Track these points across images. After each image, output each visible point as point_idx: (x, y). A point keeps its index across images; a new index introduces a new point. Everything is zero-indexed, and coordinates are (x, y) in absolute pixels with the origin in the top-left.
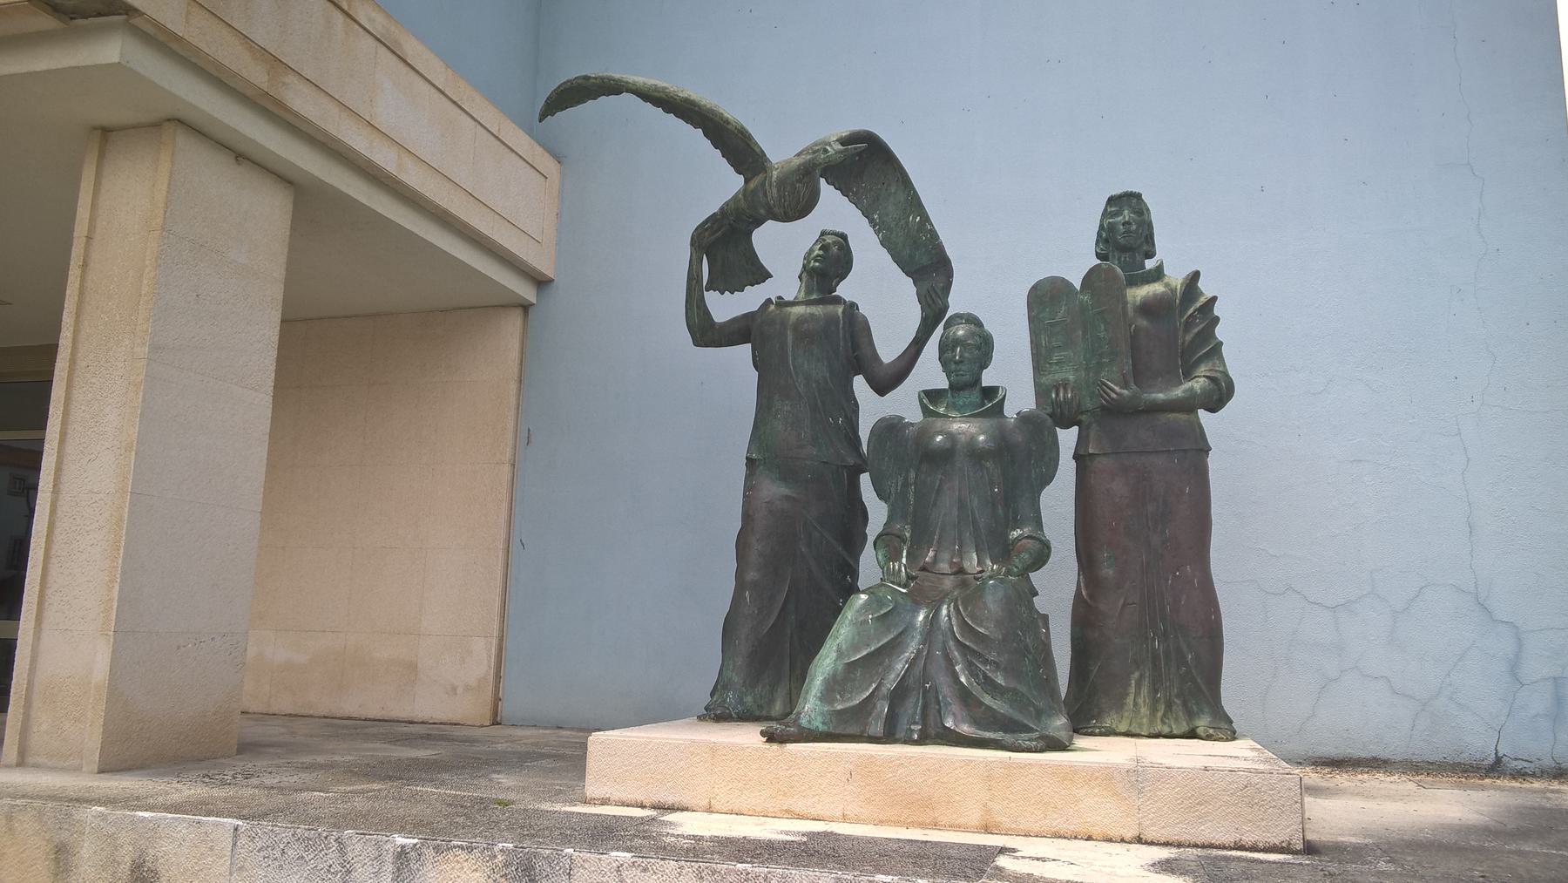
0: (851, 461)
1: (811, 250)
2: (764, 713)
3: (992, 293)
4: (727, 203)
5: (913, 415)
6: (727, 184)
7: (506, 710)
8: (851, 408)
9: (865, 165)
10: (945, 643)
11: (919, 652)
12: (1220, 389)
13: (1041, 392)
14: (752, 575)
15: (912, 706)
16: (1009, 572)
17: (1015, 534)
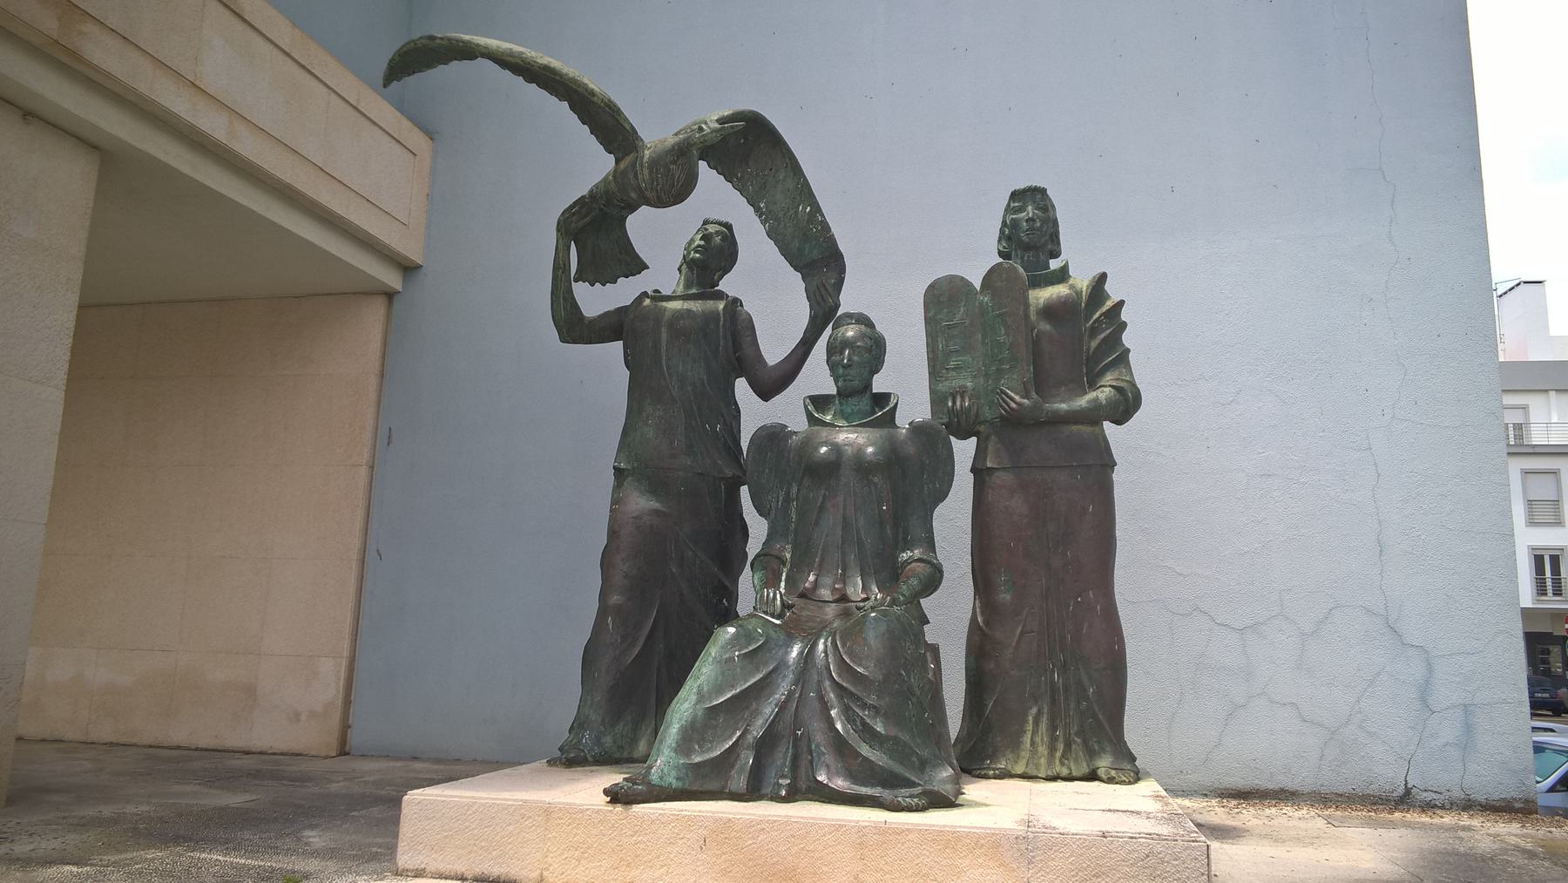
0: (729, 472)
1: (692, 240)
2: (625, 755)
3: (887, 297)
4: (596, 186)
5: (797, 422)
6: (597, 165)
7: (355, 738)
8: (733, 413)
9: (750, 148)
10: (820, 683)
11: (791, 693)
12: (1126, 400)
13: (937, 400)
14: (615, 599)
15: (782, 756)
16: (894, 602)
17: (905, 556)
